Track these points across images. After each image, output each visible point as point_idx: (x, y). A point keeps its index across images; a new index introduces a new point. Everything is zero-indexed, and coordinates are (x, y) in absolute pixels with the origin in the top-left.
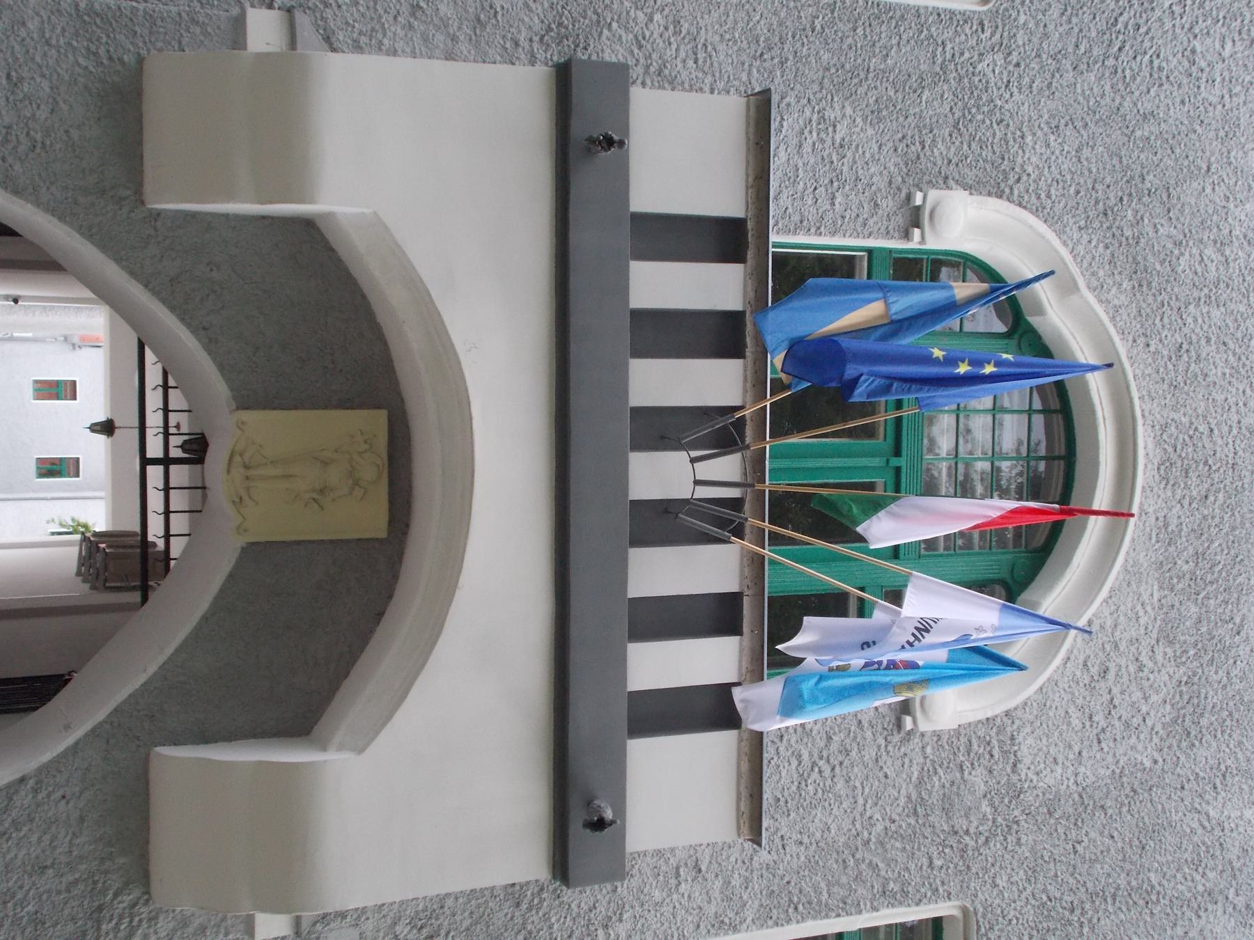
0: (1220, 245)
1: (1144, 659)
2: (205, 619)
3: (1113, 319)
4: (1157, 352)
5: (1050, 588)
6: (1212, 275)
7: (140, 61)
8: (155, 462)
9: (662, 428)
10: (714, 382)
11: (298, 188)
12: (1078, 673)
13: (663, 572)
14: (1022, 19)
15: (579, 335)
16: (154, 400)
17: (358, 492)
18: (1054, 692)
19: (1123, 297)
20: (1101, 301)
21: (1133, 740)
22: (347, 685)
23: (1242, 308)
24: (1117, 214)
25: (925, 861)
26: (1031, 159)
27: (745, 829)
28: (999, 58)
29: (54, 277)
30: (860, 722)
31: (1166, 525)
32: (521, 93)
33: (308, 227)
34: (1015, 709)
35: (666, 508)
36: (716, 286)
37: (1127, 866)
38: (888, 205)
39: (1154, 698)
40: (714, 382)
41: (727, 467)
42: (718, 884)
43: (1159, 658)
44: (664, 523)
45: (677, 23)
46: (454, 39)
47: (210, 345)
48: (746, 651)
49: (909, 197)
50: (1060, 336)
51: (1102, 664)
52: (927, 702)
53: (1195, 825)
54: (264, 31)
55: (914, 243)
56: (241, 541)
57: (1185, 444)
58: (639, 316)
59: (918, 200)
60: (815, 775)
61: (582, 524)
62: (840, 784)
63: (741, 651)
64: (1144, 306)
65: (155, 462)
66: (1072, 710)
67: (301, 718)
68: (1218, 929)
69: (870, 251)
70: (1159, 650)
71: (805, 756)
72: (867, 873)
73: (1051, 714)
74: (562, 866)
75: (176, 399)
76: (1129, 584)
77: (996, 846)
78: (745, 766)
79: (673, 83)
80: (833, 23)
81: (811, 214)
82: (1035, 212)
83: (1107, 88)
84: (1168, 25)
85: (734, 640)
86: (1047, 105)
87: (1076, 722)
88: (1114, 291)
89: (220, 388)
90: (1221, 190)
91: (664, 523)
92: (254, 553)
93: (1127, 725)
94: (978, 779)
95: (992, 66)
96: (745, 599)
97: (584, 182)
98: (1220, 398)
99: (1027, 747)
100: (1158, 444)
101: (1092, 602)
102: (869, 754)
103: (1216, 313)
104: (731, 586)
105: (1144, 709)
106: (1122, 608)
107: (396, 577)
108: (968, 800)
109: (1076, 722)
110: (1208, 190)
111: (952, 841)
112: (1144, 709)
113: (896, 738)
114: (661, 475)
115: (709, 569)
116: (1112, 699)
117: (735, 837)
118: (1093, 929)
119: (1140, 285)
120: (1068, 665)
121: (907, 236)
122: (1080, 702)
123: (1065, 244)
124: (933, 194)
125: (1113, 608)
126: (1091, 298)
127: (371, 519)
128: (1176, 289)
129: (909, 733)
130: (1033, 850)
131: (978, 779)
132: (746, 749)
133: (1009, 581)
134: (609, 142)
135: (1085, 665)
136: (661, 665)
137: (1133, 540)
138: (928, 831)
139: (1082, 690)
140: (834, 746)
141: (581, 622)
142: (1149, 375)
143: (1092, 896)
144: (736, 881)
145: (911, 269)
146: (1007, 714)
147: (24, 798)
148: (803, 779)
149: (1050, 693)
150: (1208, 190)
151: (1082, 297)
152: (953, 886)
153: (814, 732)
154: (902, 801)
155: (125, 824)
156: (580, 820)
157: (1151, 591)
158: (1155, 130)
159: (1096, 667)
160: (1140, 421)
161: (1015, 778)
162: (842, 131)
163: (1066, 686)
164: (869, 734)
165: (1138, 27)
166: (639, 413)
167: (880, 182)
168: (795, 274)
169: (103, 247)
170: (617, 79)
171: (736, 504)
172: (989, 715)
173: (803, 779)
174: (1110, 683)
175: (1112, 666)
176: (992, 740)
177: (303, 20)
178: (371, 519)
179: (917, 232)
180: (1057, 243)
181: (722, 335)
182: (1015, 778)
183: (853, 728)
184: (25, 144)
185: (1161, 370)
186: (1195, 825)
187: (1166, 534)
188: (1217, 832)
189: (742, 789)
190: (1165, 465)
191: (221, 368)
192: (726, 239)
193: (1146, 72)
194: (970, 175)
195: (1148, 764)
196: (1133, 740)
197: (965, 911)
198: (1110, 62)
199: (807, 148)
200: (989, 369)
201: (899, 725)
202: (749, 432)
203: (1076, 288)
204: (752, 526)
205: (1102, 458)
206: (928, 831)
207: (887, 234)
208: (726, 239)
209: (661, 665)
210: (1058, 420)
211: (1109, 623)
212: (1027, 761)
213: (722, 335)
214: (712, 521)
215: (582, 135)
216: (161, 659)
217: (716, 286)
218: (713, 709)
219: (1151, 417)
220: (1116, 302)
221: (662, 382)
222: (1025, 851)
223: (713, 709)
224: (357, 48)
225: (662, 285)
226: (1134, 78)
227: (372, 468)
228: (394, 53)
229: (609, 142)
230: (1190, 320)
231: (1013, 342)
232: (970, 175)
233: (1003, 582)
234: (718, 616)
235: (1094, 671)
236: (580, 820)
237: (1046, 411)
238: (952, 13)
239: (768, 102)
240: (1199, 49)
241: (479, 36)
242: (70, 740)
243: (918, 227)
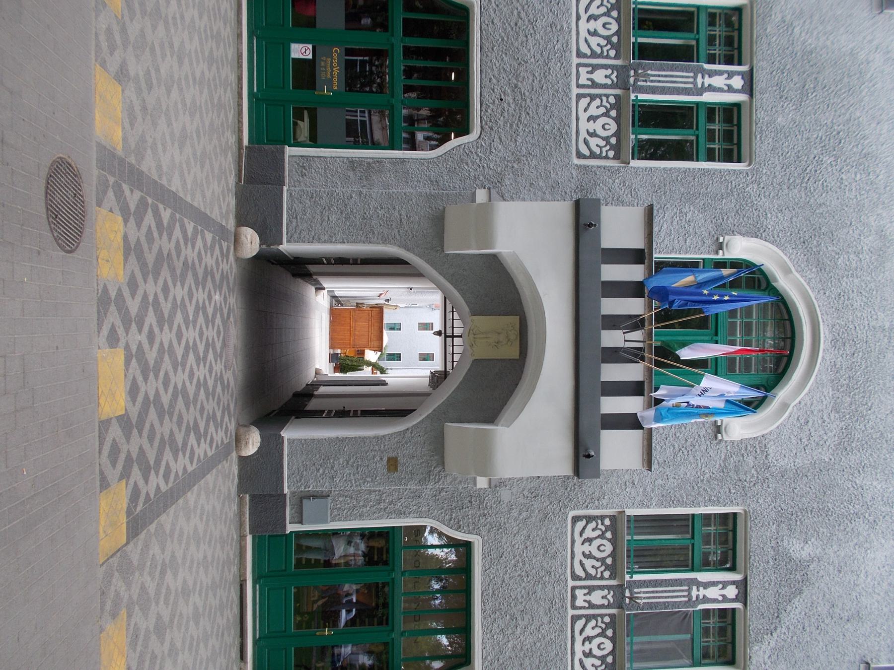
0: (857, 254)
1: (825, 418)
2: (461, 383)
3: (808, 284)
5: (782, 388)
6: (854, 265)
7: (444, 208)
8: (449, 337)
9: (614, 322)
10: (634, 306)
11: (489, 244)
13: (613, 372)
14: (765, 171)
15: (584, 289)
16: (449, 316)
17: (509, 343)
20: (802, 277)
21: (820, 450)
22: (505, 407)
23: (869, 279)
24: (809, 243)
25: (727, 490)
26: (770, 223)
27: (646, 465)
28: (755, 186)
29: (420, 279)
31: (835, 365)
32: (560, 212)
33: (494, 257)
35: (616, 350)
36: (634, 273)
37: (818, 500)
38: (708, 242)
39: (830, 434)
40: (634, 306)
41: (637, 335)
42: (641, 490)
43: (832, 418)
44: (614, 355)
45: (624, 182)
46: (544, 193)
47: (463, 295)
49: (718, 239)
50: (785, 290)
53: (850, 486)
54: (481, 196)
55: (720, 256)
56: (472, 359)
57: (843, 333)
58: (605, 283)
59: (721, 240)
60: (681, 453)
61: (585, 356)
62: (691, 458)
65: (449, 337)
67: (491, 416)
68: (860, 529)
69: (703, 259)
70: (832, 415)
71: (676, 446)
72: (702, 492)
74: (577, 471)
75: (456, 316)
77: (758, 486)
78: (645, 443)
79: (623, 203)
80: (685, 177)
81: (677, 246)
82: (772, 243)
83: (803, 195)
84: (830, 169)
86: (776, 202)
87: (794, 441)
89: (467, 309)
90: (857, 232)
91: (614, 355)
92: (476, 362)
93: (818, 444)
94: (750, 460)
95: (752, 189)
97: (585, 238)
98: (859, 315)
99: (771, 449)
100: (831, 332)
102: (703, 447)
103: (856, 281)
104: (640, 378)
105: (825, 438)
107: (522, 372)
108: (746, 468)
109: (794, 441)
110: (851, 232)
111: (739, 483)
112: (825, 438)
113: (715, 442)
114: (613, 338)
117: (641, 467)
118: (801, 523)
121: (717, 253)
123: (786, 255)
124: (727, 237)
127: (514, 353)
129: (720, 441)
130: (775, 490)
131: (750, 460)
134: (590, 225)
136: (612, 405)
137: (819, 370)
138: (728, 479)
140: (688, 443)
141: (584, 390)
143: (801, 510)
144: (648, 489)
145: (720, 264)
146: (763, 436)
147: (408, 435)
148: (675, 455)
150: (851, 232)
152: (740, 501)
154: (717, 466)
155: (438, 446)
156: (583, 456)
157: (829, 391)
158: (826, 210)
160: (821, 323)
161: (766, 461)
162: (689, 216)
164: (703, 440)
165: (816, 171)
166: (605, 317)
167: (705, 234)
168: (662, 266)
169: (432, 266)
170: (596, 204)
171: (640, 349)
173: (675, 455)
176: (758, 446)
177: (493, 191)
178: (514, 353)
179: (721, 252)
180: (782, 255)
181: (636, 289)
182: (766, 461)
184: (411, 236)
186: (850, 486)
187: (835, 368)
188: (860, 489)
190: (834, 341)
191: (466, 302)
192: (637, 256)
193: (820, 188)
194: (744, 230)
195: (827, 460)
196: (820, 450)
197: (745, 511)
198: (804, 185)
199: (675, 223)
200: (726, 298)
201: (716, 438)
202: (646, 324)
203: (791, 272)
206: (728, 479)
207: (709, 253)
208: (637, 256)
209: (612, 405)
211: (809, 403)
212: (772, 455)
213: (636, 289)
215: (584, 222)
216: (448, 395)
217: (634, 273)
218: (631, 422)
221: (613, 306)
222: (771, 490)
223: (631, 422)
224: (512, 199)
225: (613, 272)
226: (815, 190)
227: (514, 335)
228: (524, 200)
229: (590, 225)
230: (844, 284)
231: (767, 293)
232: (744, 230)
233: (763, 386)
234: (636, 389)
235: (802, 421)
236: (583, 456)
238: (735, 171)
239: (652, 208)
240: (844, 178)
241: (552, 192)
242: (421, 419)
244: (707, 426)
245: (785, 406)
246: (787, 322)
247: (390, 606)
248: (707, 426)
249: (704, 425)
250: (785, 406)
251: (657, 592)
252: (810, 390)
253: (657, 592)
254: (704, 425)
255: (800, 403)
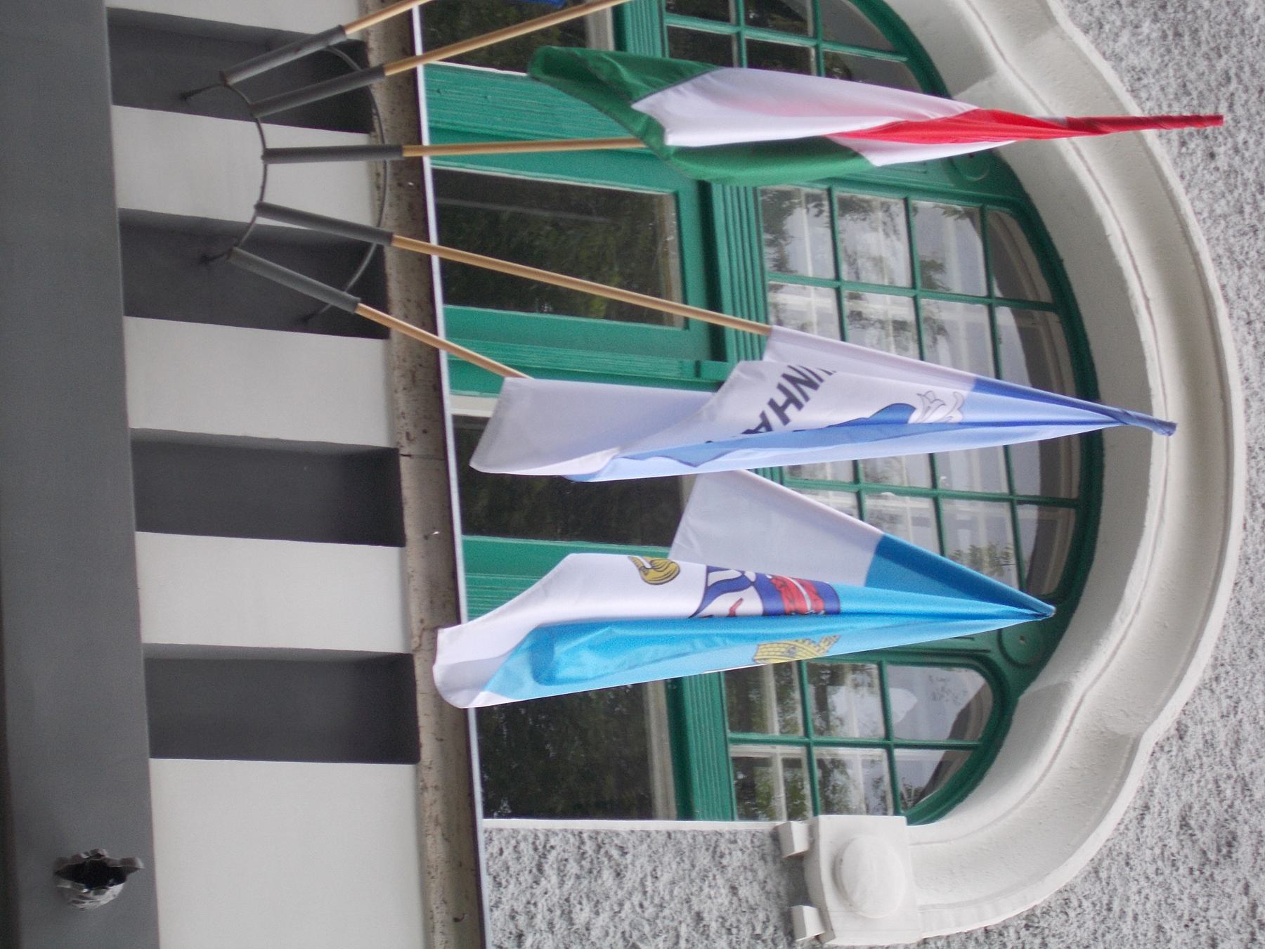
4: (1232, 172)
5: (1087, 654)
12: (1173, 843)
18: (1126, 881)
19: (1145, 53)
30: (699, 917)
34: (1046, 913)
48: (417, 582)
51: (1221, 825)
52: (846, 870)
59: (799, 844)
63: (405, 578)
64: (1192, 76)
66: (1170, 924)
73: (1126, 929)
76: (1251, 654)
78: (437, 850)
85: (401, 772)
88: (1125, 37)
96: (404, 463)
101: (1179, 679)
106: (1245, 704)
115: (319, 391)
116: (1254, 907)
119: (1178, 35)
120: (1147, 821)
122: (1184, 906)
125: (1225, 703)
126: (1084, 42)
128: (1248, 51)
132: (437, 810)
133: (996, 656)
135: (1184, 824)
137: (1245, 559)
139: (1187, 882)
142: (1225, 216)
149: (1117, 882)
151: (1063, 36)
153: (595, 933)
159: (1209, 832)
163: (1151, 871)
172: (992, 921)
174: (1245, 870)
175: (1243, 831)
179: (809, 915)
183: (683, 930)
185: (1248, 209)
189: (435, 899)
204: (403, 252)
205: (1154, 381)
210: (1066, 520)
214: (320, 280)
219: (1245, 304)
220: (1133, 60)
235: (1206, 838)
237: (1046, 501)
243: (808, 901)
244: (735, 860)
245: (1112, 753)
246: (1053, 318)
247: (268, 54)
248: (735, 860)
249: (717, 855)
250: (1112, 753)
251: (741, 300)
252: (1217, 663)
253: (741, 300)
254: (717, 855)
255: (1181, 732)
